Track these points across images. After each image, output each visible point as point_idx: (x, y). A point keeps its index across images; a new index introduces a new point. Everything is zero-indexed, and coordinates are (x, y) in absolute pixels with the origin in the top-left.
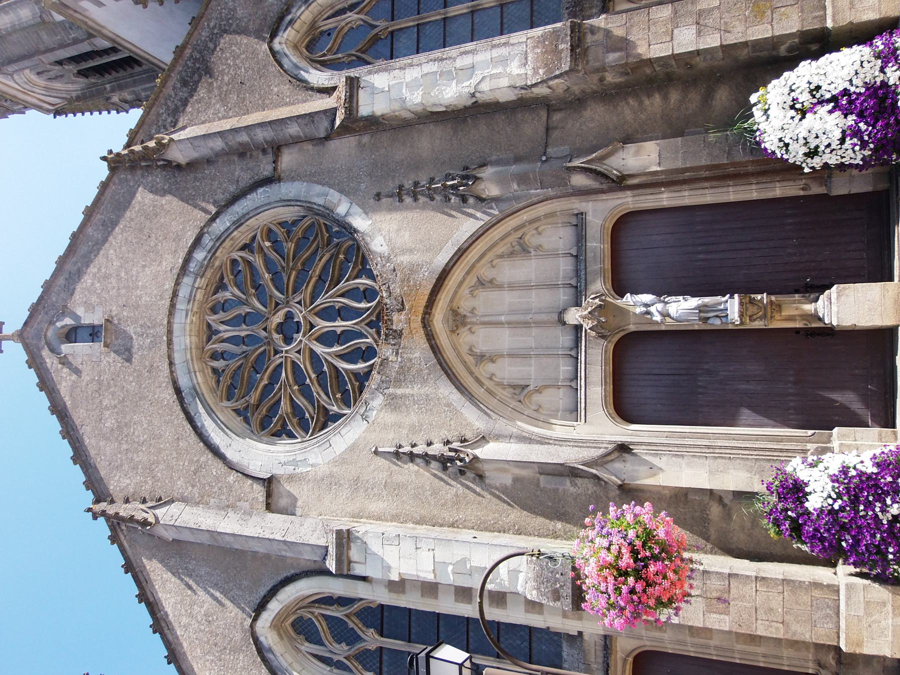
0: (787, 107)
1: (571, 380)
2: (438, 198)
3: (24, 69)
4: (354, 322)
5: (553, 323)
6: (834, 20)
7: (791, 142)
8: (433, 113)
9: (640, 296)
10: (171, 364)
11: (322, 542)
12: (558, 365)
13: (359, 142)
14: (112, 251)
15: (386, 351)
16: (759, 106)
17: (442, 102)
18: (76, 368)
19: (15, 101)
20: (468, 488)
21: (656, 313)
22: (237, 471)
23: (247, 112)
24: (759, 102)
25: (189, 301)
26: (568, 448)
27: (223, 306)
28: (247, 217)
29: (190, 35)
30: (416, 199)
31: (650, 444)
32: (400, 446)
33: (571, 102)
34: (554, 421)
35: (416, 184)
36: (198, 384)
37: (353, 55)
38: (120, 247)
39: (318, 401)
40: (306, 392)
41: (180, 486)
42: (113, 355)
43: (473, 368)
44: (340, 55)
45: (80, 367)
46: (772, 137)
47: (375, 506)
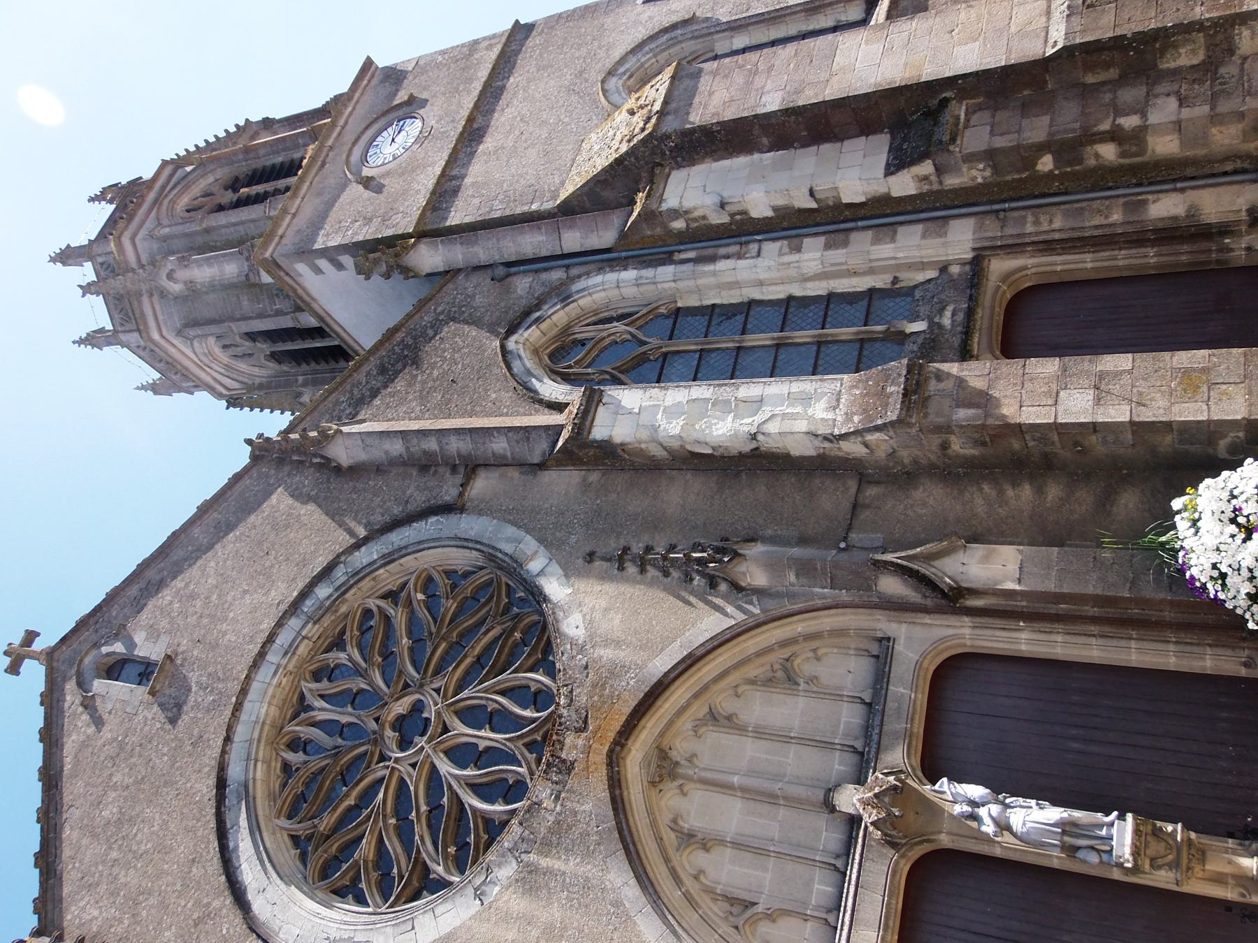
1: (829, 911)
2: (675, 574)
3: (207, 335)
5: (812, 804)
9: (964, 785)
10: (228, 739)
12: (812, 880)
13: (584, 479)
14: (213, 564)
15: (542, 791)
16: (1185, 515)
17: (708, 440)
21: (987, 820)
22: (259, 936)
23: (449, 416)
25: (286, 653)
28: (404, 552)
29: (409, 316)
30: (643, 571)
35: (648, 549)
36: (254, 780)
37: (607, 372)
39: (418, 852)
40: (405, 833)
42: (156, 708)
43: (671, 852)
44: (590, 370)
45: (106, 717)
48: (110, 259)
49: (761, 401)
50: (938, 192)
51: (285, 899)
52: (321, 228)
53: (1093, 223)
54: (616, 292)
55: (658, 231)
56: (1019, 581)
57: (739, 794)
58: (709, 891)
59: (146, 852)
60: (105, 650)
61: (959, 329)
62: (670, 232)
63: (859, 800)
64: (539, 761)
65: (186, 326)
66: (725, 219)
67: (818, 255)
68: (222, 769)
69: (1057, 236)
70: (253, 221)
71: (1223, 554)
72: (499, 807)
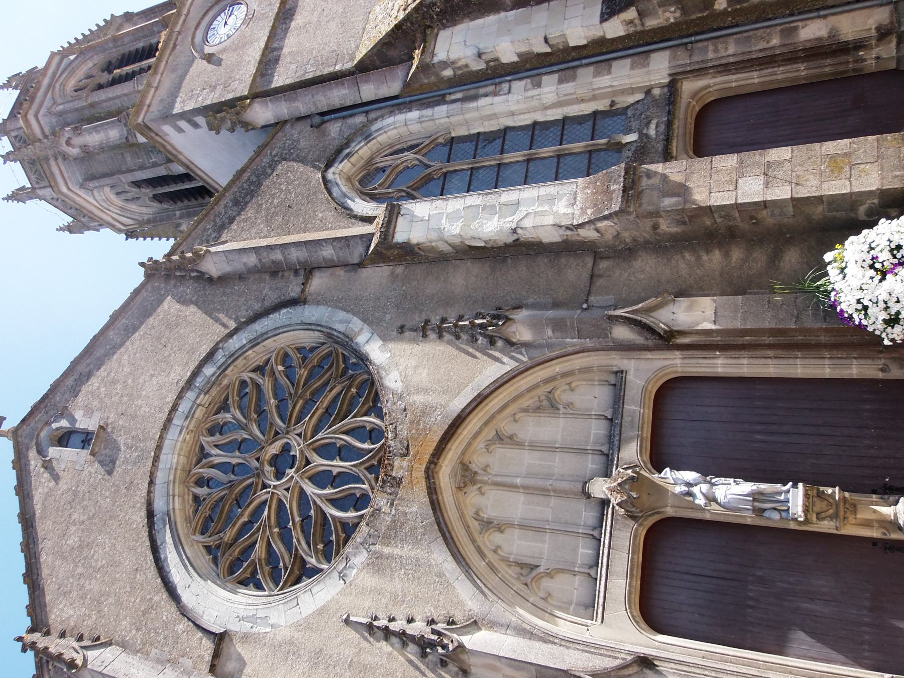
0: (867, 267)
1: (591, 567)
2: (464, 337)
4: (353, 463)
7: (870, 304)
10: (151, 482)
12: (577, 546)
14: (126, 357)
15: (380, 501)
17: (481, 236)
18: (57, 474)
19: (92, 218)
21: (699, 495)
22: (189, 619)
23: (289, 233)
24: (835, 260)
26: (576, 652)
28: (265, 336)
29: (252, 160)
30: (440, 336)
31: (680, 663)
32: (376, 618)
33: (621, 251)
34: (558, 613)
35: (444, 320)
36: (174, 509)
37: (403, 191)
39: (297, 550)
41: (125, 628)
42: (97, 465)
43: (476, 535)
44: (390, 190)
46: (849, 297)
48: (20, 133)
51: (205, 591)
54: (405, 129)
55: (433, 79)
56: (715, 322)
57: (522, 490)
58: (504, 560)
59: (102, 566)
61: (662, 137)
62: (441, 80)
63: (607, 488)
64: (377, 479)
66: (482, 66)
67: (554, 88)
68: (149, 504)
69: (731, 60)
70: (126, 95)
71: (865, 292)
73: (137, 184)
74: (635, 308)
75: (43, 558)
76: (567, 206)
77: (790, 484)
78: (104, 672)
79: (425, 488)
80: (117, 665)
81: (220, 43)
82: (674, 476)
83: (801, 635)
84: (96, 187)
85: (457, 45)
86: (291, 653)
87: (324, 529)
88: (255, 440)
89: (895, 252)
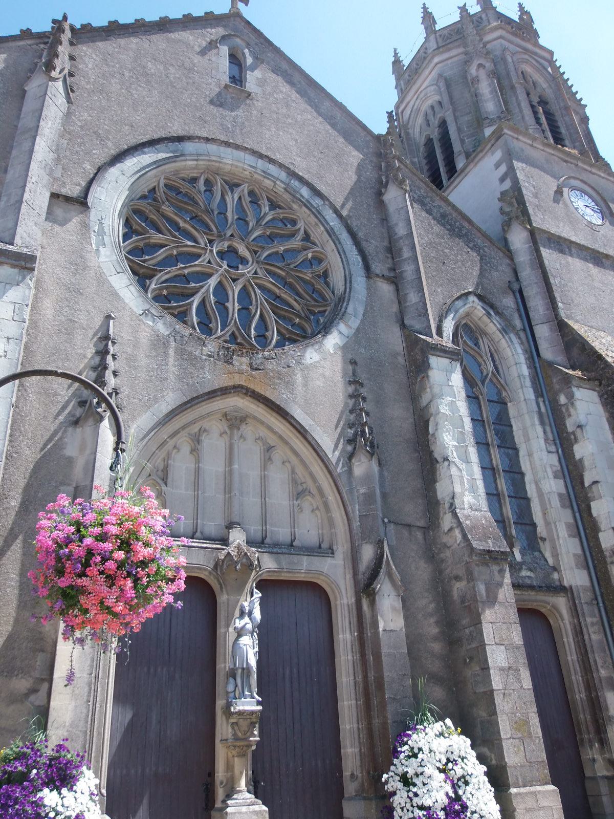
2: (352, 417)
3: (441, 95)
6: (517, 794)
7: (419, 760)
8: (427, 423)
11: (18, 240)
13: (398, 354)
15: (211, 346)
17: (439, 431)
20: (64, 408)
21: (243, 622)
22: (96, 174)
23: (423, 263)
25: (264, 172)
27: (255, 201)
29: (479, 230)
30: (351, 396)
32: (114, 343)
35: (364, 399)
36: (186, 160)
38: (312, 125)
39: (161, 271)
40: (170, 261)
42: (217, 90)
43: (187, 430)
45: (207, 57)
46: (423, 741)
47: (48, 307)
48: (485, 23)
49: (468, 462)
50: (606, 562)
51: (120, 189)
52: (526, 164)
53: (597, 658)
54: (513, 363)
55: (557, 387)
56: (384, 630)
57: (227, 469)
58: (169, 455)
59: (132, 94)
60: (246, 51)
61: (521, 581)
62: (556, 394)
63: (239, 543)
64: (226, 341)
65: (446, 80)
66: (570, 429)
67: (554, 489)
68: (189, 138)
69: (586, 637)
70: (523, 117)
71: (429, 755)
72: (195, 319)
73: (443, 124)
74: (391, 562)
75: (134, 40)
76: (469, 503)
77: (261, 699)
78: (47, 97)
79: (226, 385)
80: (53, 109)
81: (572, 202)
82: (255, 601)
83: (129, 716)
84: (440, 89)
85: (586, 405)
86: (76, 267)
87: (178, 295)
88: (248, 233)
89: (463, 780)
